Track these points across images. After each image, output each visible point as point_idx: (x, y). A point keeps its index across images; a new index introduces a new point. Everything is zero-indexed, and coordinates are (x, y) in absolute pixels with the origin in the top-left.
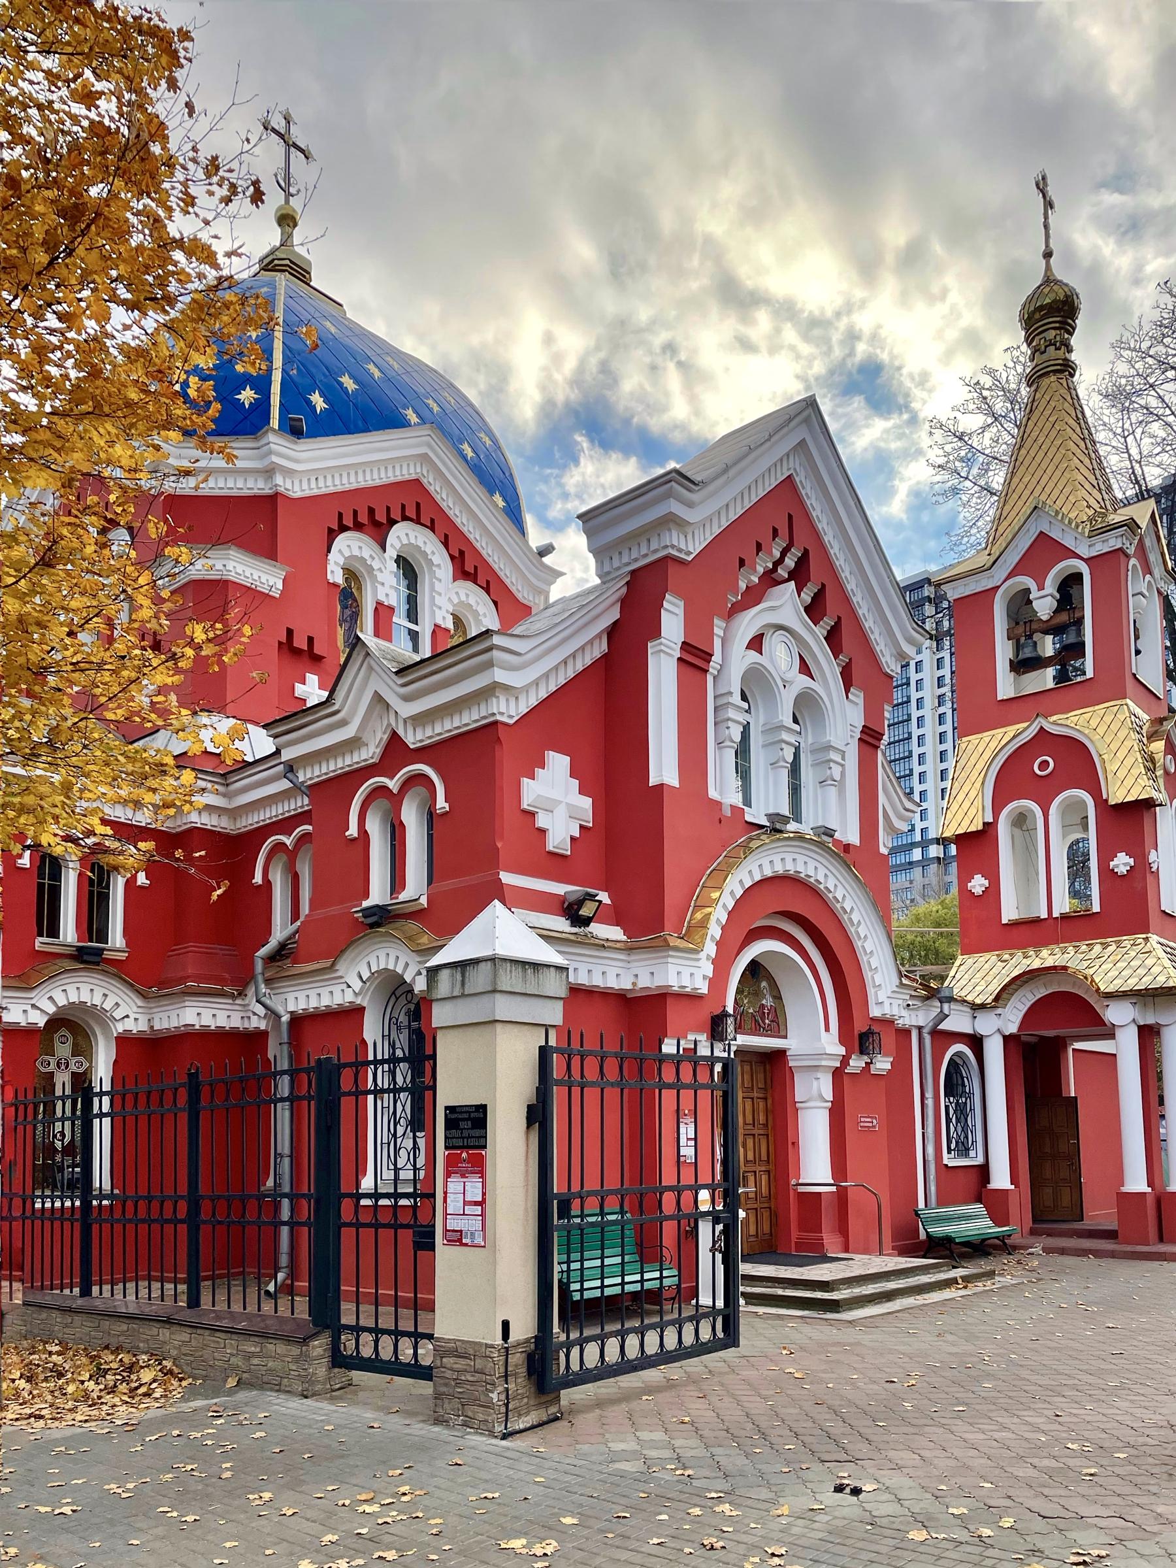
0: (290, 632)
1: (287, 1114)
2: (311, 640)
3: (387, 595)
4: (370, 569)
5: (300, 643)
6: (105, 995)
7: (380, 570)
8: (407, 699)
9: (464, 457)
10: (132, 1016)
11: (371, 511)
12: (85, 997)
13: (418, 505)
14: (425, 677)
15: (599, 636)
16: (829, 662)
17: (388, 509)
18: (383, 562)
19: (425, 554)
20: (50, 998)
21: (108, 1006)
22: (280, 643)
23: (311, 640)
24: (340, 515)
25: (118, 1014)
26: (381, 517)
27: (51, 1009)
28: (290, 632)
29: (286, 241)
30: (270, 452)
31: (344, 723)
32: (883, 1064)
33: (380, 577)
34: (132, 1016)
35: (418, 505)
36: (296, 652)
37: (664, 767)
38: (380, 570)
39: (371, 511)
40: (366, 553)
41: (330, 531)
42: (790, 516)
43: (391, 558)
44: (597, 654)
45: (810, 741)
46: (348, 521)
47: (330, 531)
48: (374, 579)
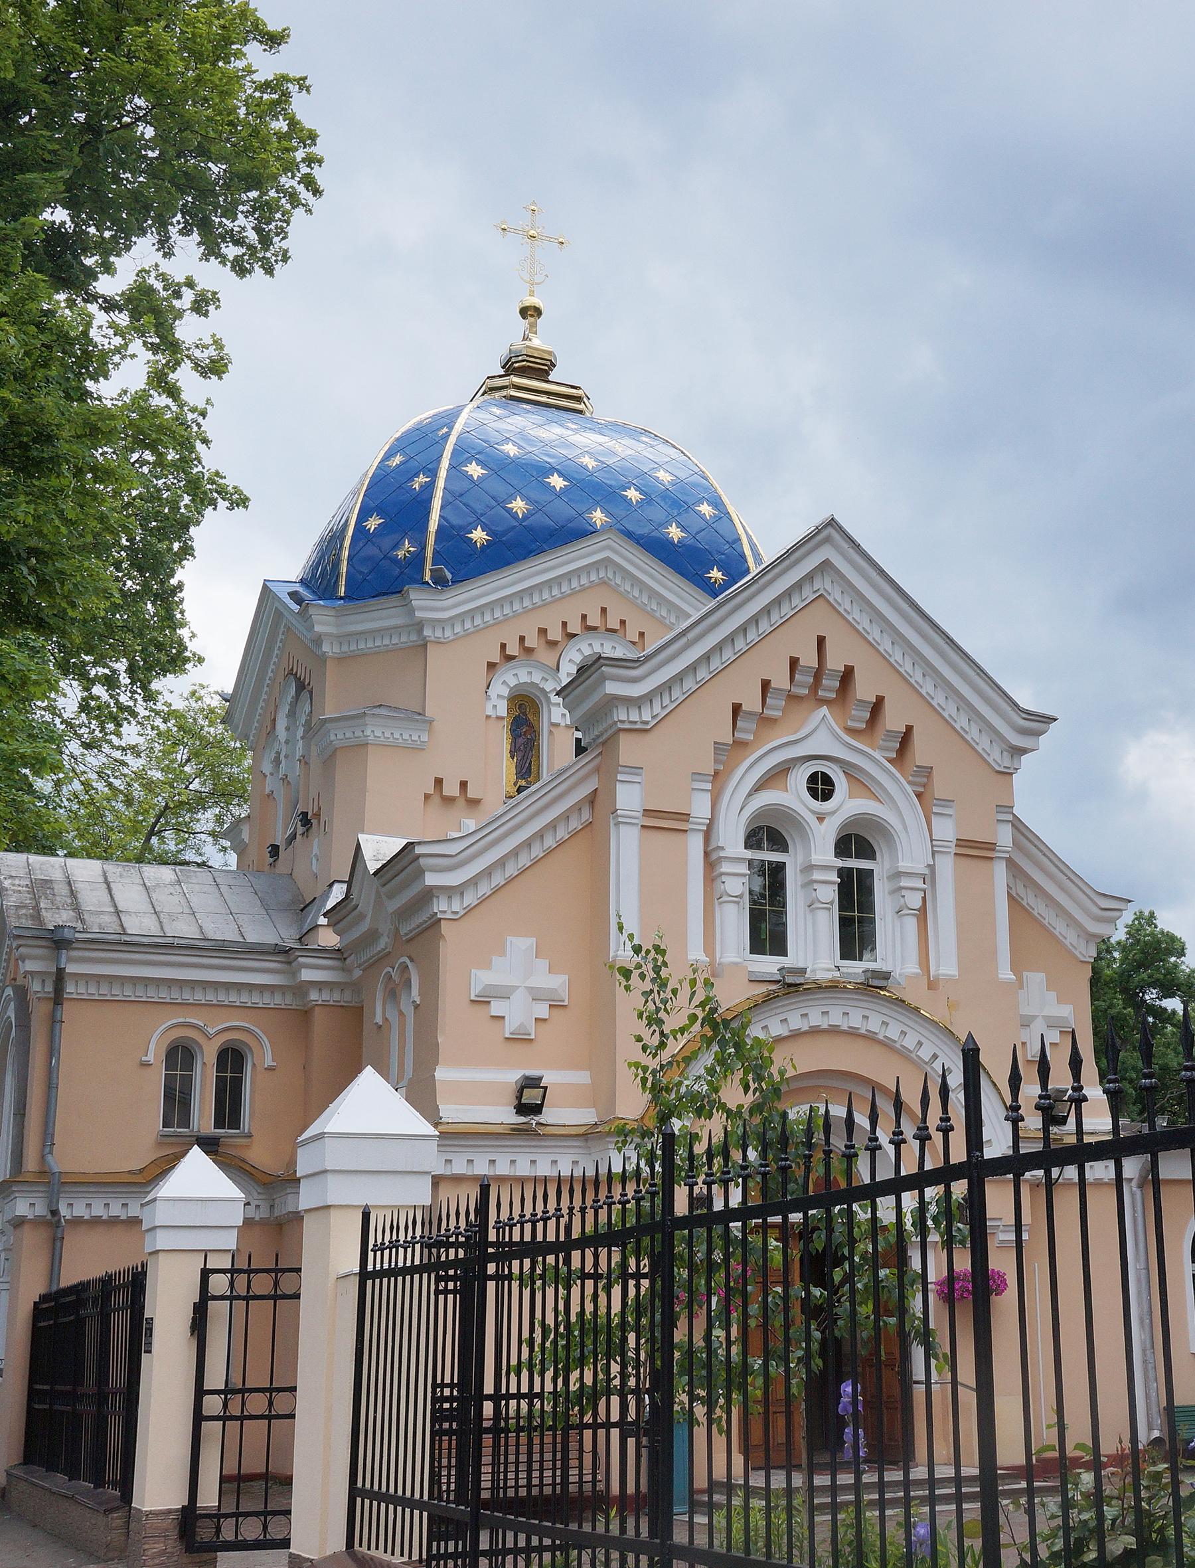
0: (439, 782)
2: (464, 785)
11: (543, 632)
13: (604, 610)
15: (577, 808)
23: (464, 785)
24: (503, 646)
26: (555, 634)
28: (439, 782)
35: (604, 610)
39: (543, 632)
40: (536, 678)
41: (491, 666)
42: (821, 641)
47: (491, 666)
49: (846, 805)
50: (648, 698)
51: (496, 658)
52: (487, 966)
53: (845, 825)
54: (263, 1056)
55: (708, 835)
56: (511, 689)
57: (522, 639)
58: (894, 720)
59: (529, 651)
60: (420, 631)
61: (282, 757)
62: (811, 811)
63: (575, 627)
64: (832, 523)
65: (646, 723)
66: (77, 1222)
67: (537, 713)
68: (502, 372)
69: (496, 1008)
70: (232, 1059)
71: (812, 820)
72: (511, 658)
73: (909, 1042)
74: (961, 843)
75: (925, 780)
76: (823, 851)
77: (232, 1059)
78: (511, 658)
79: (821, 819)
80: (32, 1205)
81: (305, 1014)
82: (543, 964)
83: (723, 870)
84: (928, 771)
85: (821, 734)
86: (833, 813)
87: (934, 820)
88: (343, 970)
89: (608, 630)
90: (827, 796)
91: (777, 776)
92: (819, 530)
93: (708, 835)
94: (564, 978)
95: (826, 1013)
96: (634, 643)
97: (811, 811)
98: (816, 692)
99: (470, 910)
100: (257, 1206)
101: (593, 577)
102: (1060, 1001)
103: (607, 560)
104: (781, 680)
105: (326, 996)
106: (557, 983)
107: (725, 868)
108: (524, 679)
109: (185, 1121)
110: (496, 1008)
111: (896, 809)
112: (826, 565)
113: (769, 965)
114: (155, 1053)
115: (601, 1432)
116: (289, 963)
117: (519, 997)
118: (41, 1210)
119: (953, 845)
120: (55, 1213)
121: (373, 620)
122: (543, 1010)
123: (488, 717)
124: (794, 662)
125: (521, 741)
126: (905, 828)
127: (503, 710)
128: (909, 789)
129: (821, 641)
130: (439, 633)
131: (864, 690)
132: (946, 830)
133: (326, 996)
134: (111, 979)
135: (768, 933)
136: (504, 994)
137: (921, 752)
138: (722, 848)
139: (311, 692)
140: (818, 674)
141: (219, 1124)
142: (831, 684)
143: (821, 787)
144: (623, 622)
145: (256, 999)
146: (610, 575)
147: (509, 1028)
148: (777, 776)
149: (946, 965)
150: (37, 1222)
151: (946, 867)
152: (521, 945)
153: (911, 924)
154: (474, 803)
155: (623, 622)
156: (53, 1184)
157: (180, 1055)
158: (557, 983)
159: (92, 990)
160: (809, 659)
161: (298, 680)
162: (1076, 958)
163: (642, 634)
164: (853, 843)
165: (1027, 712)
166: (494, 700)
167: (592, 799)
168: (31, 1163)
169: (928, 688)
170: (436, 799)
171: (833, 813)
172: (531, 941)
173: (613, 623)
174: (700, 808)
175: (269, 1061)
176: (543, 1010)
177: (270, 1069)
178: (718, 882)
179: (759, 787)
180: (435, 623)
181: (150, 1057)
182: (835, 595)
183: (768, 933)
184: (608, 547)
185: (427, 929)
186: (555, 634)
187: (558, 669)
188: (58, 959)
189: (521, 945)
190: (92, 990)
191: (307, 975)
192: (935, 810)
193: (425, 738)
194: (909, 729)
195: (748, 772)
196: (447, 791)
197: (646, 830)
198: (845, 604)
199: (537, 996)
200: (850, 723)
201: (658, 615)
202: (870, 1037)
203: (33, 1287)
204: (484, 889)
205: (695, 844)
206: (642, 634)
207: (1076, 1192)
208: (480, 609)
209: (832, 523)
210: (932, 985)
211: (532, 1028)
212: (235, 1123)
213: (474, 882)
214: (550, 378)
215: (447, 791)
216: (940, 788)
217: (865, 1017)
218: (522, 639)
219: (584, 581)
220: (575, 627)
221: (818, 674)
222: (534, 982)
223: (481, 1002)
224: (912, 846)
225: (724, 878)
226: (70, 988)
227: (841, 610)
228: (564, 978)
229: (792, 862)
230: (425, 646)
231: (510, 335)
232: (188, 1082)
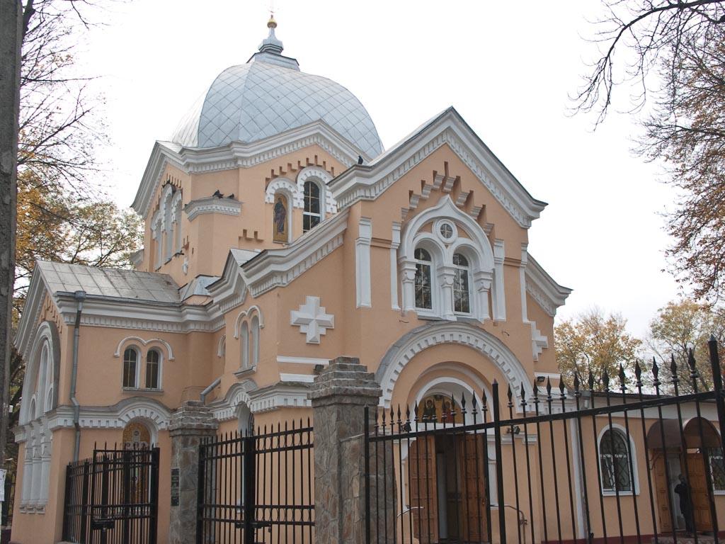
0: (245, 231)
1: (691, 450)
2: (256, 233)
3: (299, 203)
4: (290, 192)
5: (250, 235)
6: (152, 413)
7: (295, 192)
8: (248, 277)
9: (152, 236)
10: (165, 422)
11: (290, 165)
12: (143, 414)
13: (316, 157)
14: (255, 265)
15: (337, 237)
16: (479, 229)
17: (299, 162)
18: (297, 188)
19: (321, 179)
20: (127, 415)
21: (153, 418)
22: (240, 238)
23: (256, 233)
24: (273, 171)
25: (158, 421)
26: (295, 167)
27: (127, 420)
28: (245, 231)
29: (272, 33)
30: (234, 152)
31: (230, 287)
32: (3, 465)
33: (295, 195)
34: (165, 422)
35: (316, 157)
36: (249, 240)
37: (364, 298)
38: (295, 192)
39: (290, 165)
40: (287, 186)
41: (267, 180)
42: (446, 164)
43: (301, 185)
44: (336, 245)
45: (473, 269)
46: (277, 172)
47: (267, 180)
48: (292, 196)
49: (457, 241)
50: (374, 186)
51: (269, 176)
52: (297, 309)
53: (456, 250)
54: (168, 353)
55: (398, 251)
56: (308, 178)
57: (281, 168)
58: (477, 202)
59: (283, 173)
60: (236, 162)
61: (162, 222)
62: (444, 243)
63: (303, 164)
64: (452, 109)
65: (373, 197)
66: (87, 428)
67: (286, 202)
68: (259, 51)
69: (303, 329)
70: (153, 356)
71: (443, 246)
72: (276, 176)
73: (487, 349)
74: (507, 259)
75: (490, 230)
76: (448, 260)
77: (153, 356)
78: (276, 176)
79: (447, 246)
80: (66, 420)
81: (186, 336)
82: (323, 309)
83: (406, 267)
84: (492, 227)
85: (447, 207)
86: (452, 243)
87: (495, 248)
88: (205, 315)
89: (318, 166)
90: (449, 236)
91: (427, 226)
92: (447, 112)
93: (398, 251)
94: (332, 316)
95: (452, 335)
96: (329, 172)
97: (444, 243)
98: (443, 189)
99: (291, 283)
100: (167, 423)
101: (312, 141)
102: (542, 334)
103: (318, 134)
104: (429, 181)
105: (197, 327)
106: (329, 318)
107: (407, 266)
108: (281, 186)
109: (132, 384)
110: (303, 329)
111: (479, 241)
112: (449, 129)
113: (424, 312)
114: (120, 353)
115: (228, 504)
116: (181, 312)
117: (313, 324)
118: (70, 423)
119: (503, 260)
120: (77, 425)
121: (213, 157)
122: (323, 331)
123: (266, 203)
124: (435, 173)
125: (279, 214)
126: (483, 252)
127: (272, 200)
128: (485, 234)
129: (446, 164)
130: (245, 164)
131: (465, 187)
132: (501, 253)
133: (197, 327)
134: (100, 317)
135: (423, 298)
136: (306, 322)
137: (489, 217)
138: (406, 257)
139: (182, 190)
140: (444, 180)
141: (147, 387)
142: (450, 184)
143: (446, 231)
144: (324, 163)
145: (170, 329)
146: (319, 141)
147: (309, 338)
148: (427, 226)
149: (501, 316)
150: (69, 429)
151: (500, 270)
152: (313, 300)
153: (485, 295)
154: (260, 241)
155: (324, 163)
156: (77, 410)
157: (131, 354)
158: (329, 318)
159: (92, 322)
160: (441, 172)
161: (173, 186)
162: (548, 315)
163: (332, 168)
164: (461, 258)
165: (536, 201)
166: (269, 195)
167: (344, 233)
168: (63, 399)
169: (492, 188)
170: (244, 239)
171: (452, 243)
172: (318, 298)
173: (320, 163)
174: (396, 238)
175: (171, 357)
176: (323, 331)
177: (171, 360)
178: (404, 272)
179: (420, 230)
180: (243, 159)
181: (118, 354)
182: (452, 143)
183: (423, 298)
184: (319, 128)
185: (269, 291)
186: (295, 167)
187: (296, 182)
188: (78, 307)
189: (313, 300)
190: (92, 322)
191: (189, 317)
192: (495, 244)
193: (239, 211)
194: (484, 206)
195: (415, 224)
196: (248, 236)
197: (374, 249)
198: (456, 147)
199: (321, 324)
200: (457, 203)
201: (339, 159)
202: (470, 347)
203: (68, 459)
204: (297, 274)
205: (393, 254)
206: (332, 168)
207: (641, 422)
208: (284, 146)
209: (452, 109)
210: (495, 324)
211: (318, 338)
212: (155, 385)
213: (292, 269)
214: (282, 54)
215: (248, 236)
216: (498, 234)
217: (460, 336)
218: (281, 168)
219: (308, 143)
220: (303, 164)
221: (444, 180)
222: (319, 318)
223: (296, 326)
224: (488, 259)
225: (406, 271)
226: (82, 321)
227: (454, 150)
228: (332, 316)
229: (433, 266)
230: (238, 169)
231: (263, 34)
232: (133, 366)
